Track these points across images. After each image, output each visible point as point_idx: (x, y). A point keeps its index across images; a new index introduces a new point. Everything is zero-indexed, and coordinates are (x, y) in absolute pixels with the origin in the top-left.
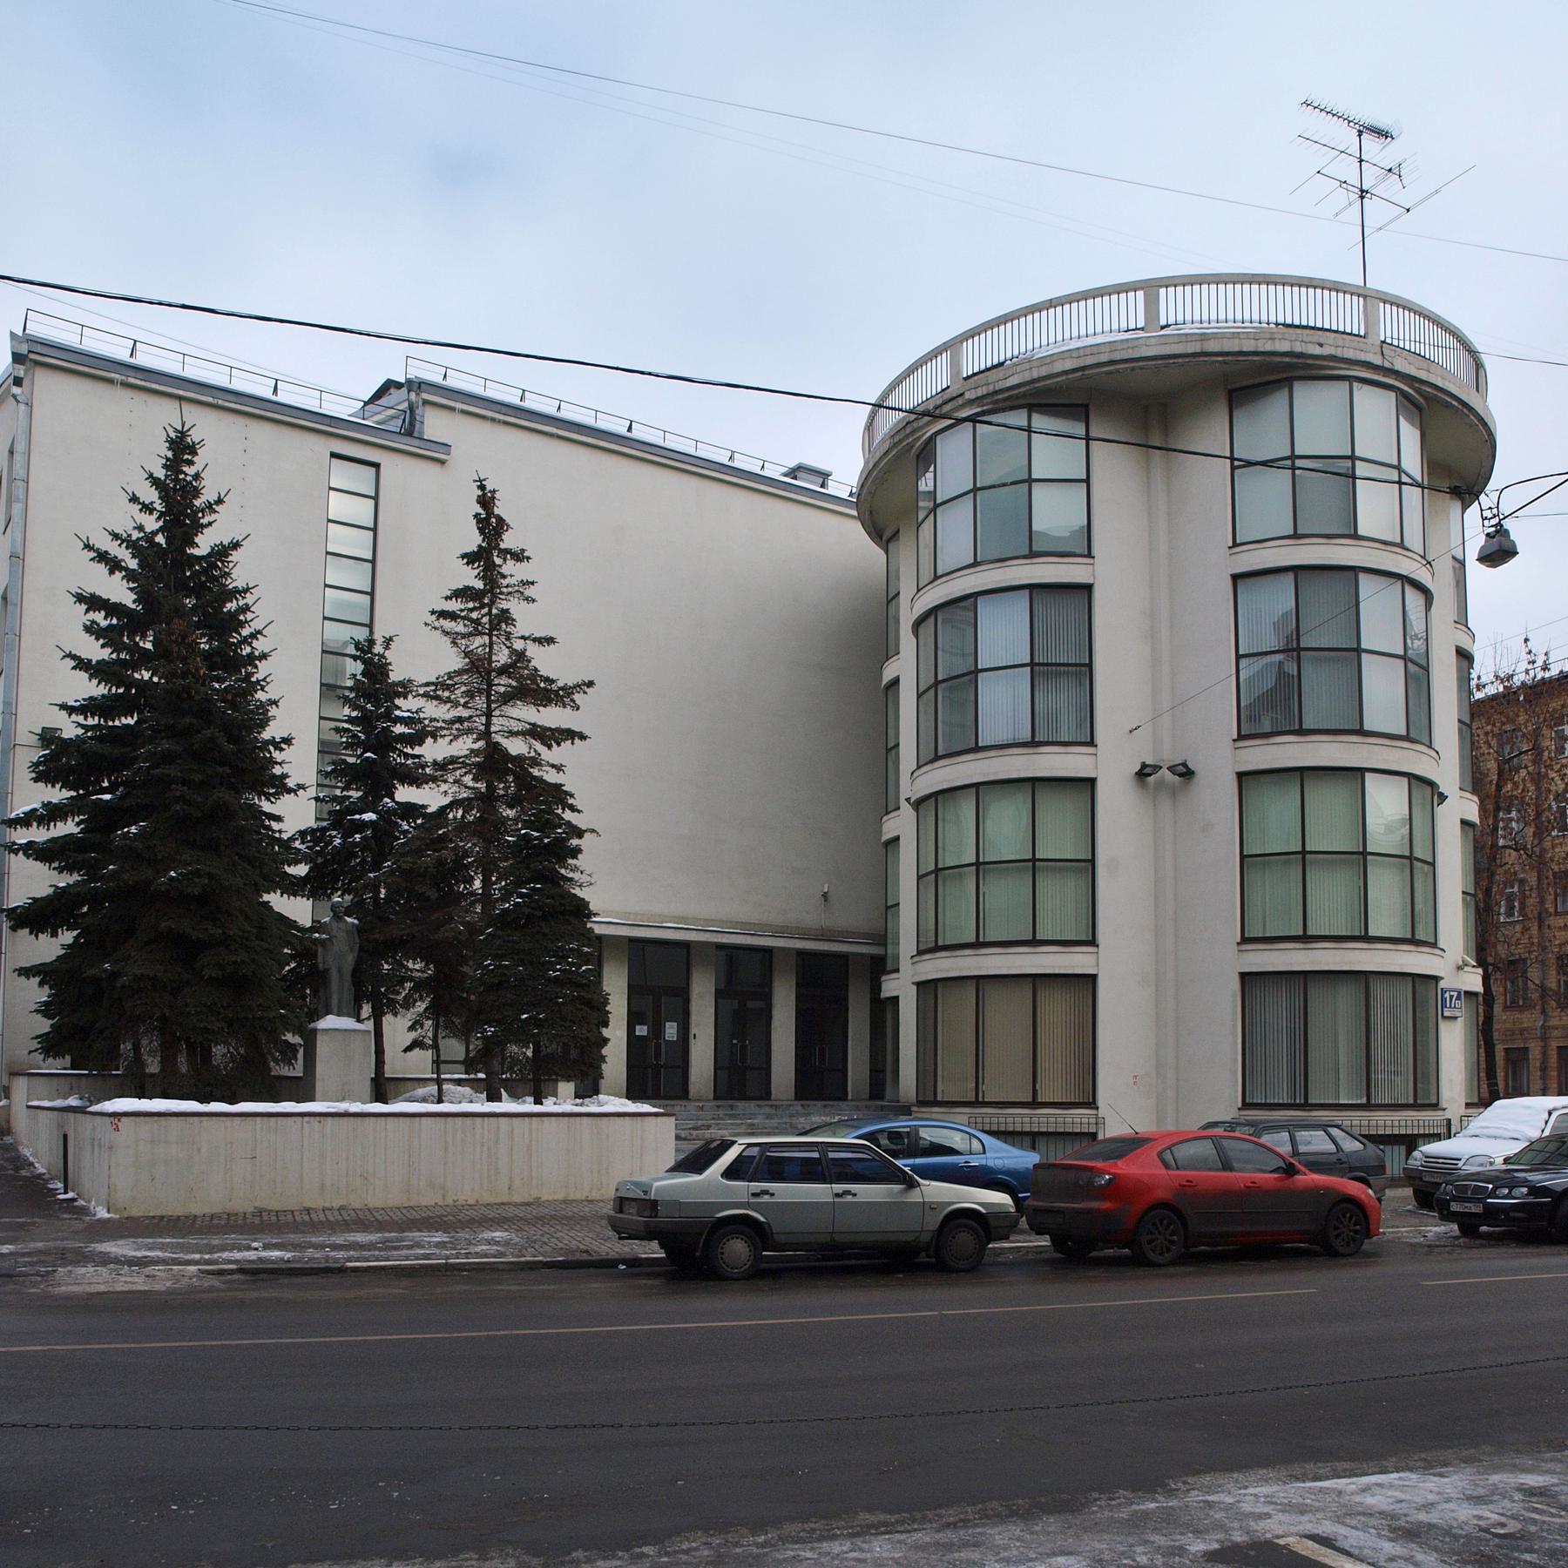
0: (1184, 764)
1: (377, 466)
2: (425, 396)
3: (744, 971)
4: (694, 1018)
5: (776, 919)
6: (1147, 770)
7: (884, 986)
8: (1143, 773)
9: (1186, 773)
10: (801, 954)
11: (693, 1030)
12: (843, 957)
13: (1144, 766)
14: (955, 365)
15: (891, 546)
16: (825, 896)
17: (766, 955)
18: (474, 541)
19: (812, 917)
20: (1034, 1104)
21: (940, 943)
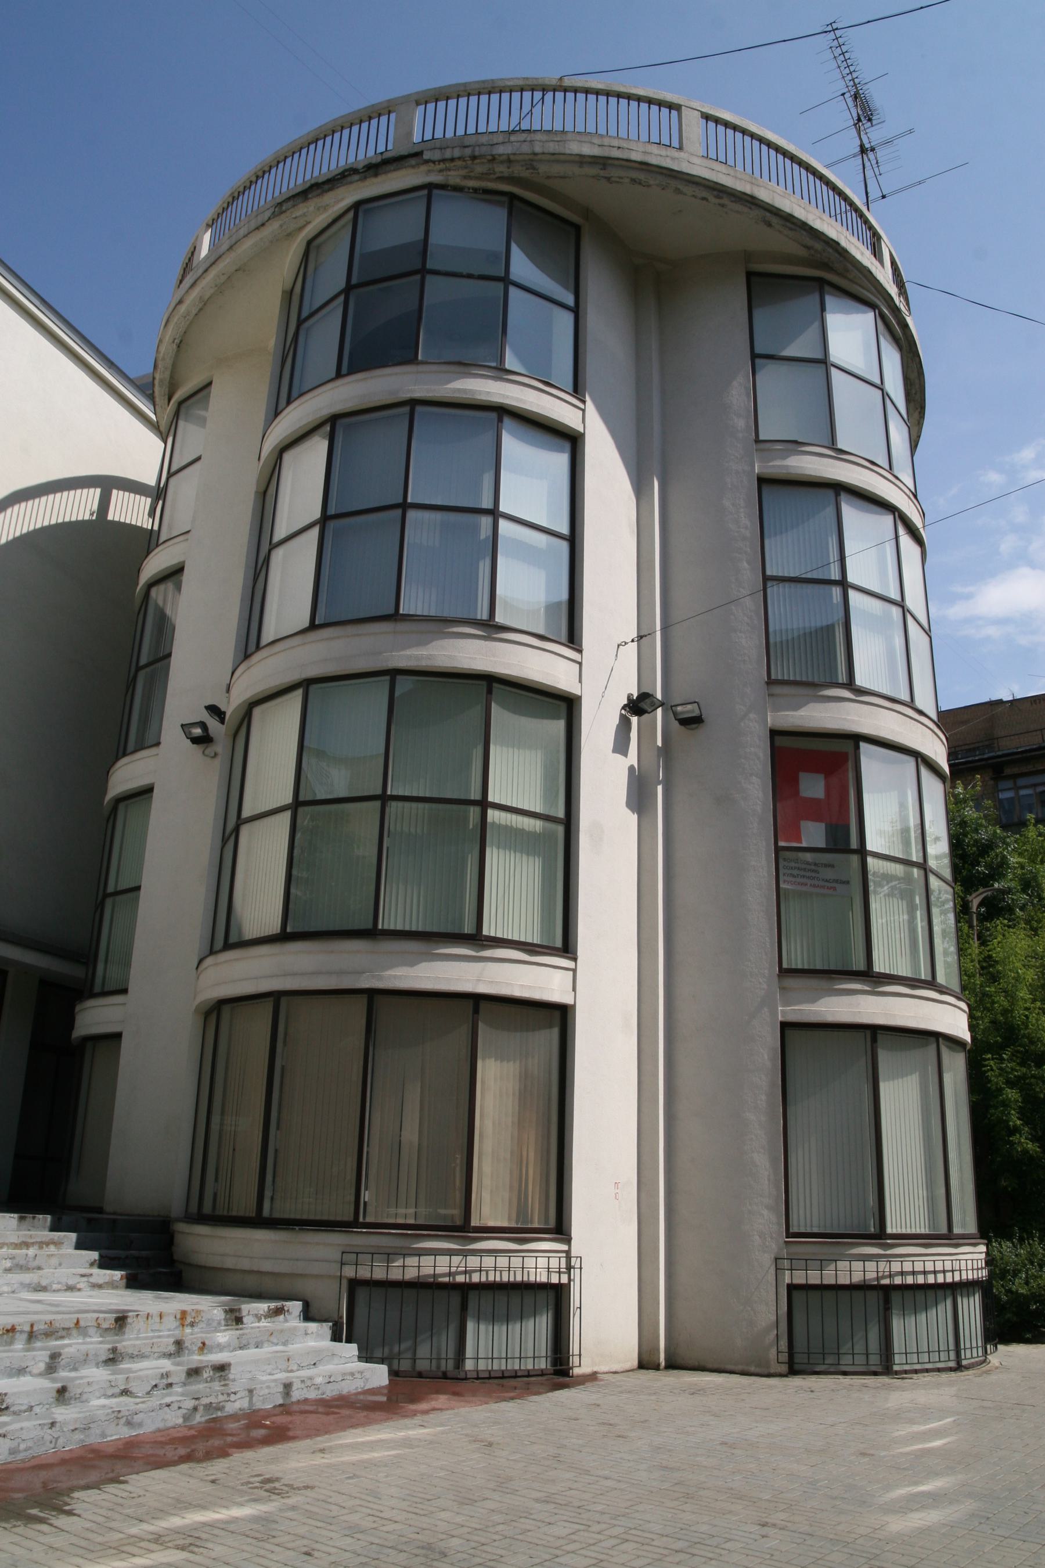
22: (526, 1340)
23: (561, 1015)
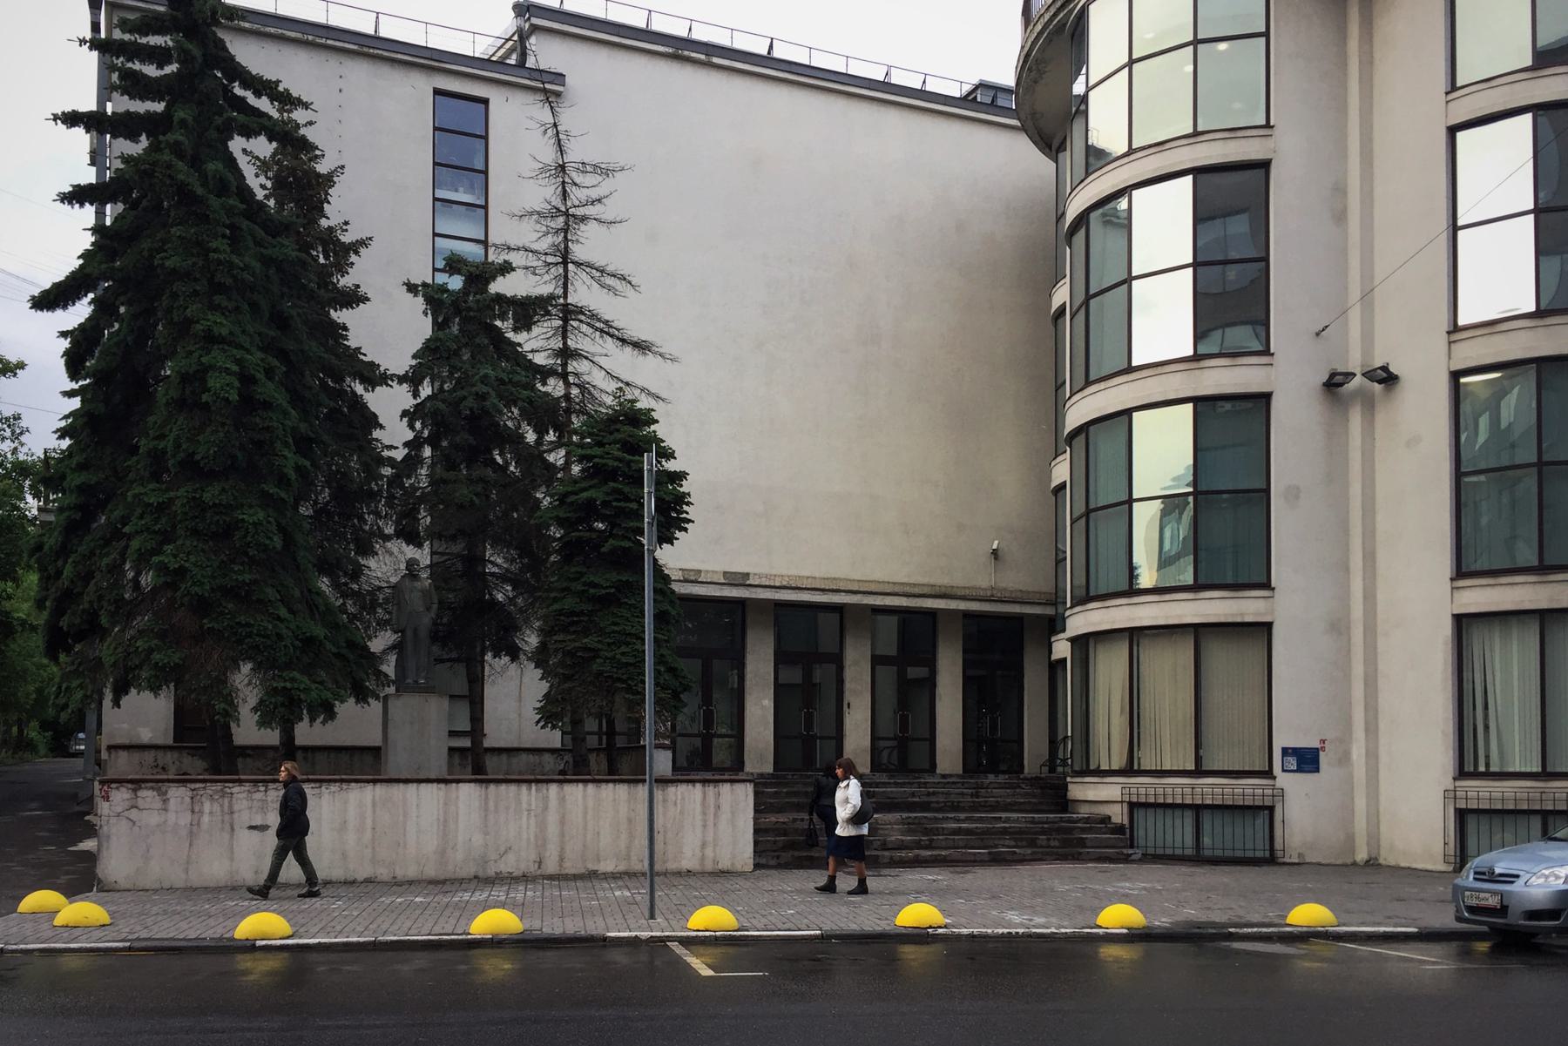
0: (1385, 368)
1: (485, 102)
2: (535, 21)
3: (910, 632)
4: (848, 685)
5: (942, 580)
6: (1338, 379)
7: (1055, 646)
8: (1334, 384)
9: (1387, 378)
10: (967, 615)
11: (848, 697)
12: (1020, 618)
13: (1333, 375)
15: (1061, 155)
16: (995, 553)
17: (739, 607)
18: (549, 155)
19: (983, 579)
20: (1199, 772)
21: (1092, 593)
22: (1247, 837)
23: (1262, 630)
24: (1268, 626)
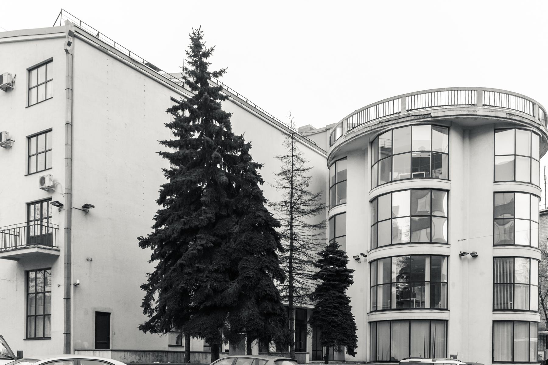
14: (404, 103)
24: (447, 321)
